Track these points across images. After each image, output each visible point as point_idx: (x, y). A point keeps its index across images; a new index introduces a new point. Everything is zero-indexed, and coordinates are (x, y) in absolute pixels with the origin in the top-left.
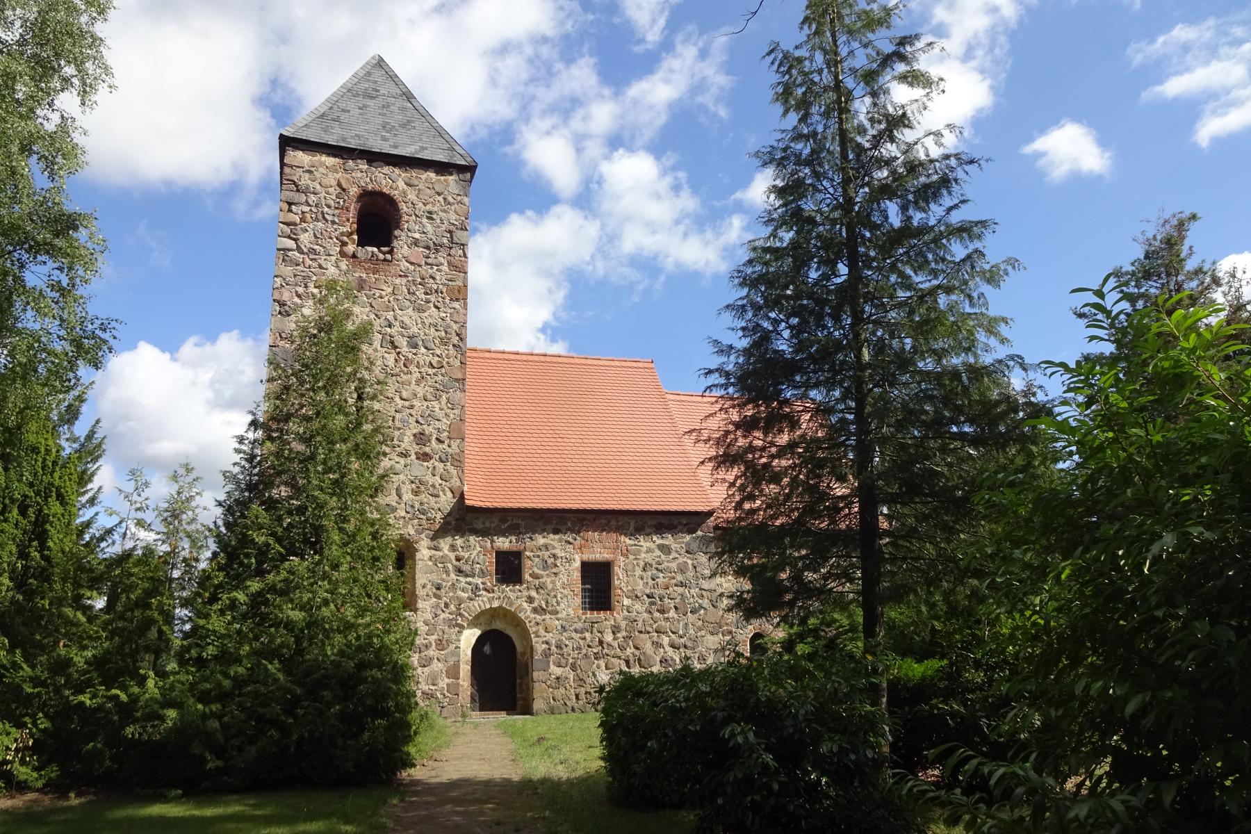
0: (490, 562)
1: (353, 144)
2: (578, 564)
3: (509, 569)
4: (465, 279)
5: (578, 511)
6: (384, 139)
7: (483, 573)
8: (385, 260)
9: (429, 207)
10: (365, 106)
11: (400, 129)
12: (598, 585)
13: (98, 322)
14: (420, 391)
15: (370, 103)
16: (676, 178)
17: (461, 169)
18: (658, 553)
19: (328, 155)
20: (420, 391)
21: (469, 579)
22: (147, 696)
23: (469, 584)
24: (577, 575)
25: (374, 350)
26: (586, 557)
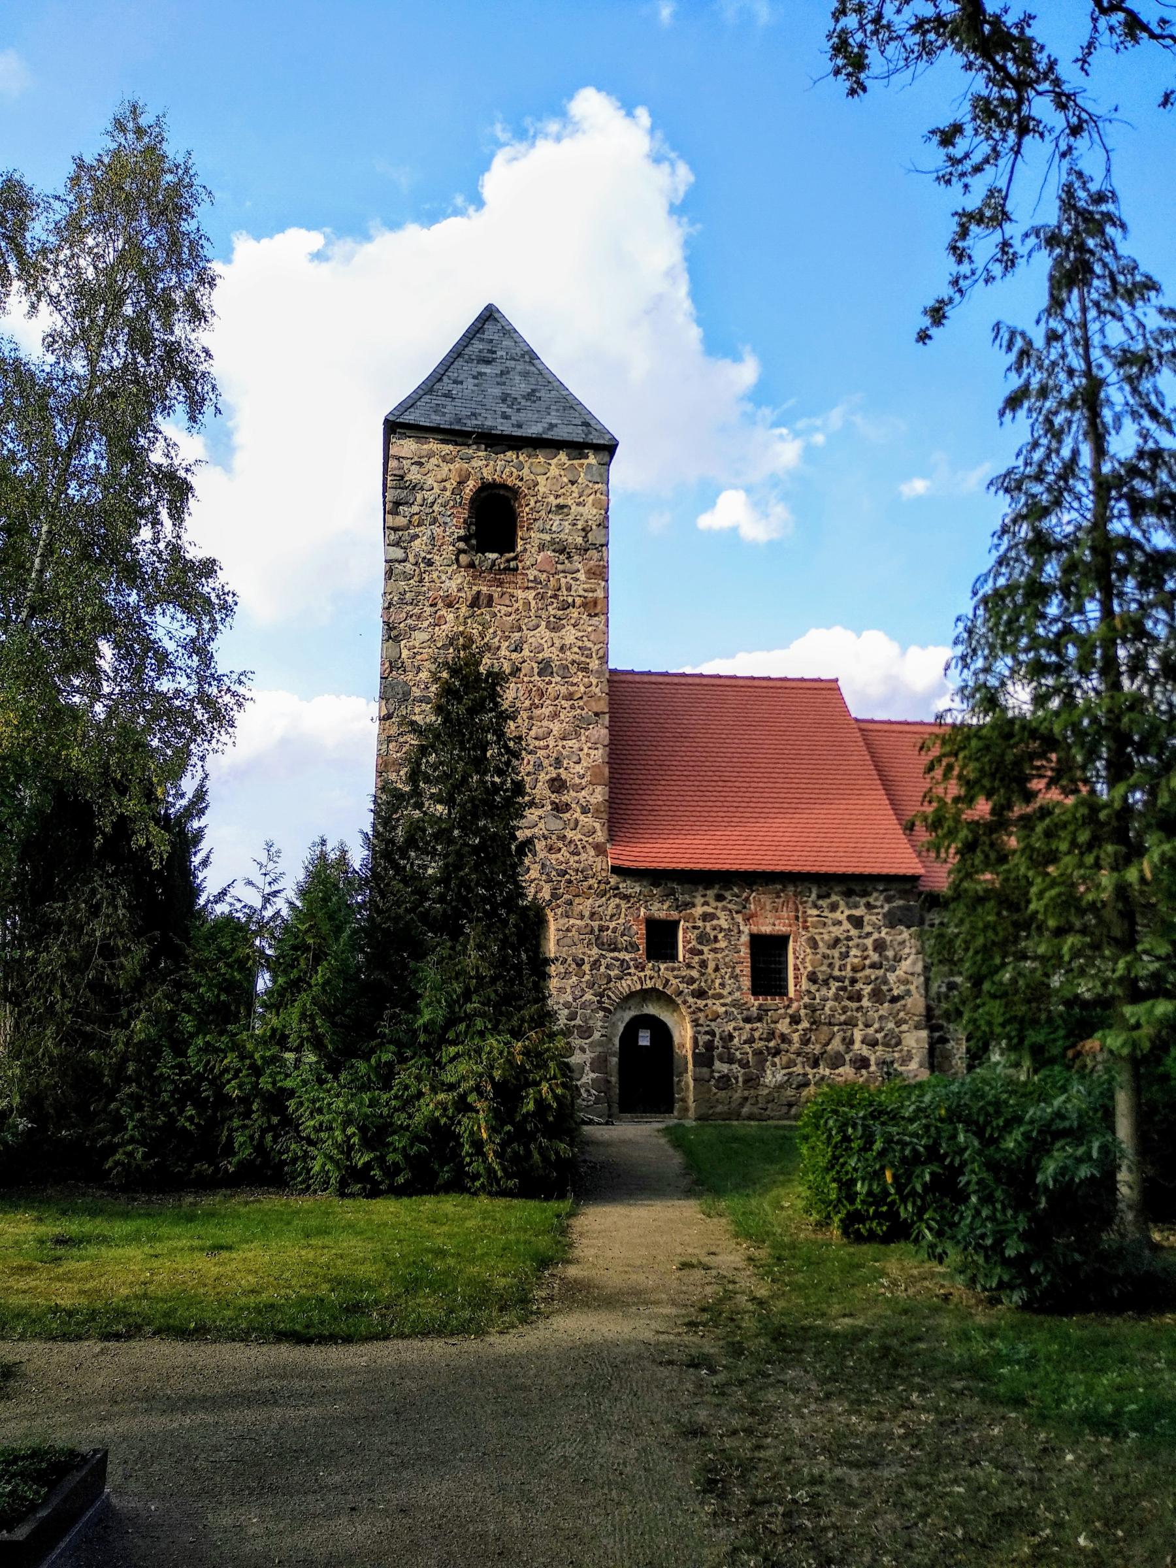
0: (639, 932)
1: (470, 425)
2: (745, 938)
3: (661, 940)
4: (606, 589)
5: (457, 353)
6: (505, 416)
7: (633, 947)
8: (507, 569)
9: (561, 501)
10: (481, 374)
11: (523, 402)
12: (768, 955)
13: (235, 676)
14: (556, 727)
15: (487, 370)
16: (1105, 889)
17: (597, 448)
18: (847, 925)
19: (444, 442)
20: (556, 727)
21: (616, 954)
22: (207, 925)
23: (617, 959)
24: (745, 952)
25: (510, 694)
26: (755, 929)
